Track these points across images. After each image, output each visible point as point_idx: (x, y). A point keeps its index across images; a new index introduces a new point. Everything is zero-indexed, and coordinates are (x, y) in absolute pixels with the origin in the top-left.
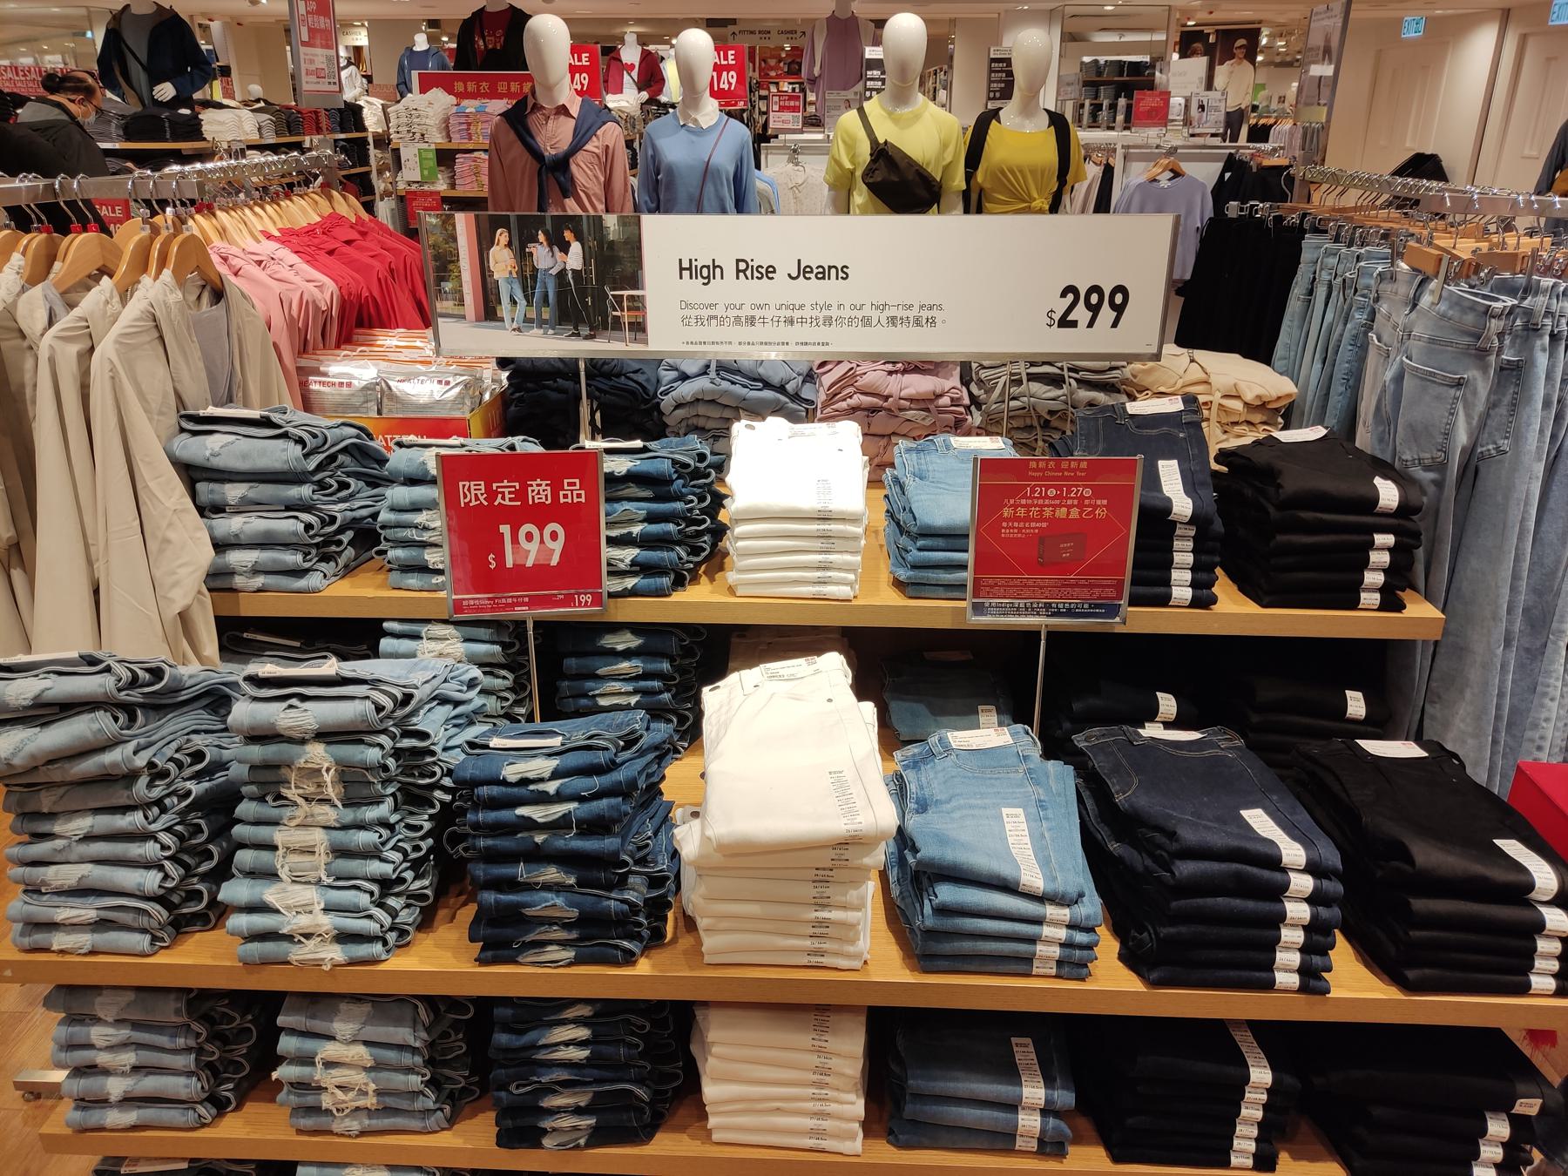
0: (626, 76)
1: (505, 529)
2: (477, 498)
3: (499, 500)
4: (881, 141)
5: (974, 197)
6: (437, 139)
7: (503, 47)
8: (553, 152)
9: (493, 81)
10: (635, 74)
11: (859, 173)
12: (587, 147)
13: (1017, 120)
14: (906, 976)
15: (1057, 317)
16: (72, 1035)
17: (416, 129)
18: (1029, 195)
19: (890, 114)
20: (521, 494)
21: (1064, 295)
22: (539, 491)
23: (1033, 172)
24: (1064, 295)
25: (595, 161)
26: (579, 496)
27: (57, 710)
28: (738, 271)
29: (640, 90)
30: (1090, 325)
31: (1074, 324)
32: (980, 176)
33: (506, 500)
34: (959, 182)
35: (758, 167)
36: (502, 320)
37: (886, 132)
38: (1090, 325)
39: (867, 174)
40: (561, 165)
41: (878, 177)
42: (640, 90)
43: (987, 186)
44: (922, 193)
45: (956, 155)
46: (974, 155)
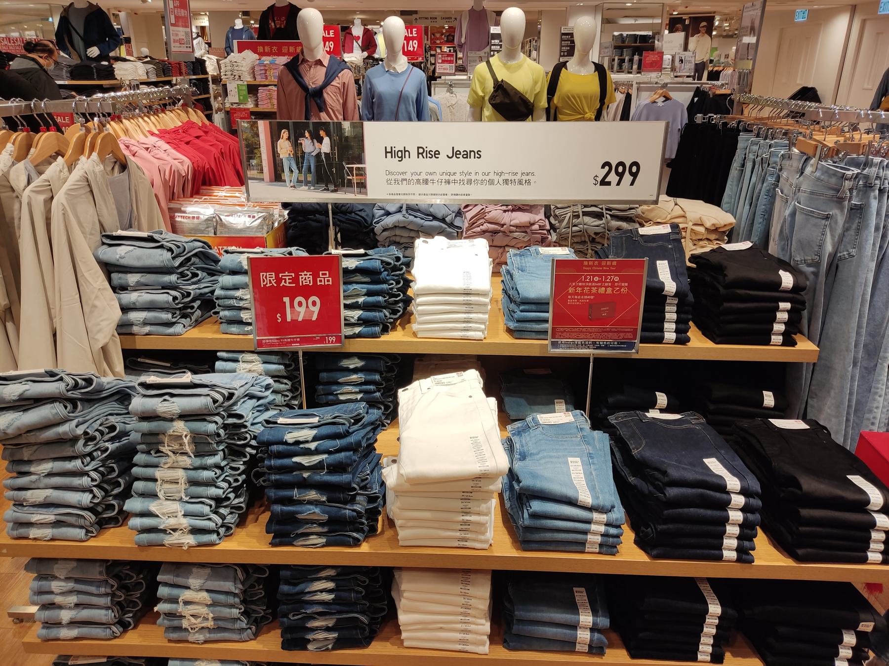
0: (355, 43)
1: (286, 300)
2: (270, 282)
3: (283, 283)
4: (500, 80)
5: (552, 112)
6: (248, 79)
7: (285, 27)
8: (314, 86)
9: (280, 46)
10: (360, 42)
11: (487, 98)
12: (333, 83)
13: (577, 68)
14: (514, 553)
15: (599, 179)
16: (41, 586)
17: (236, 73)
18: (584, 110)
19: (505, 65)
20: (295, 280)
21: (603, 167)
22: (306, 278)
23: (586, 97)
24: (603, 167)
25: (338, 91)
26: (328, 281)
27: (32, 402)
28: (419, 153)
29: (363, 51)
30: (618, 184)
31: (609, 184)
32: (556, 100)
33: (287, 283)
34: (544, 103)
35: (430, 94)
37: (502, 75)
38: (618, 184)
39: (492, 98)
40: (318, 93)
41: (498, 100)
42: (363, 51)
43: (560, 105)
44: (523, 109)
45: (542, 88)
46: (552, 88)
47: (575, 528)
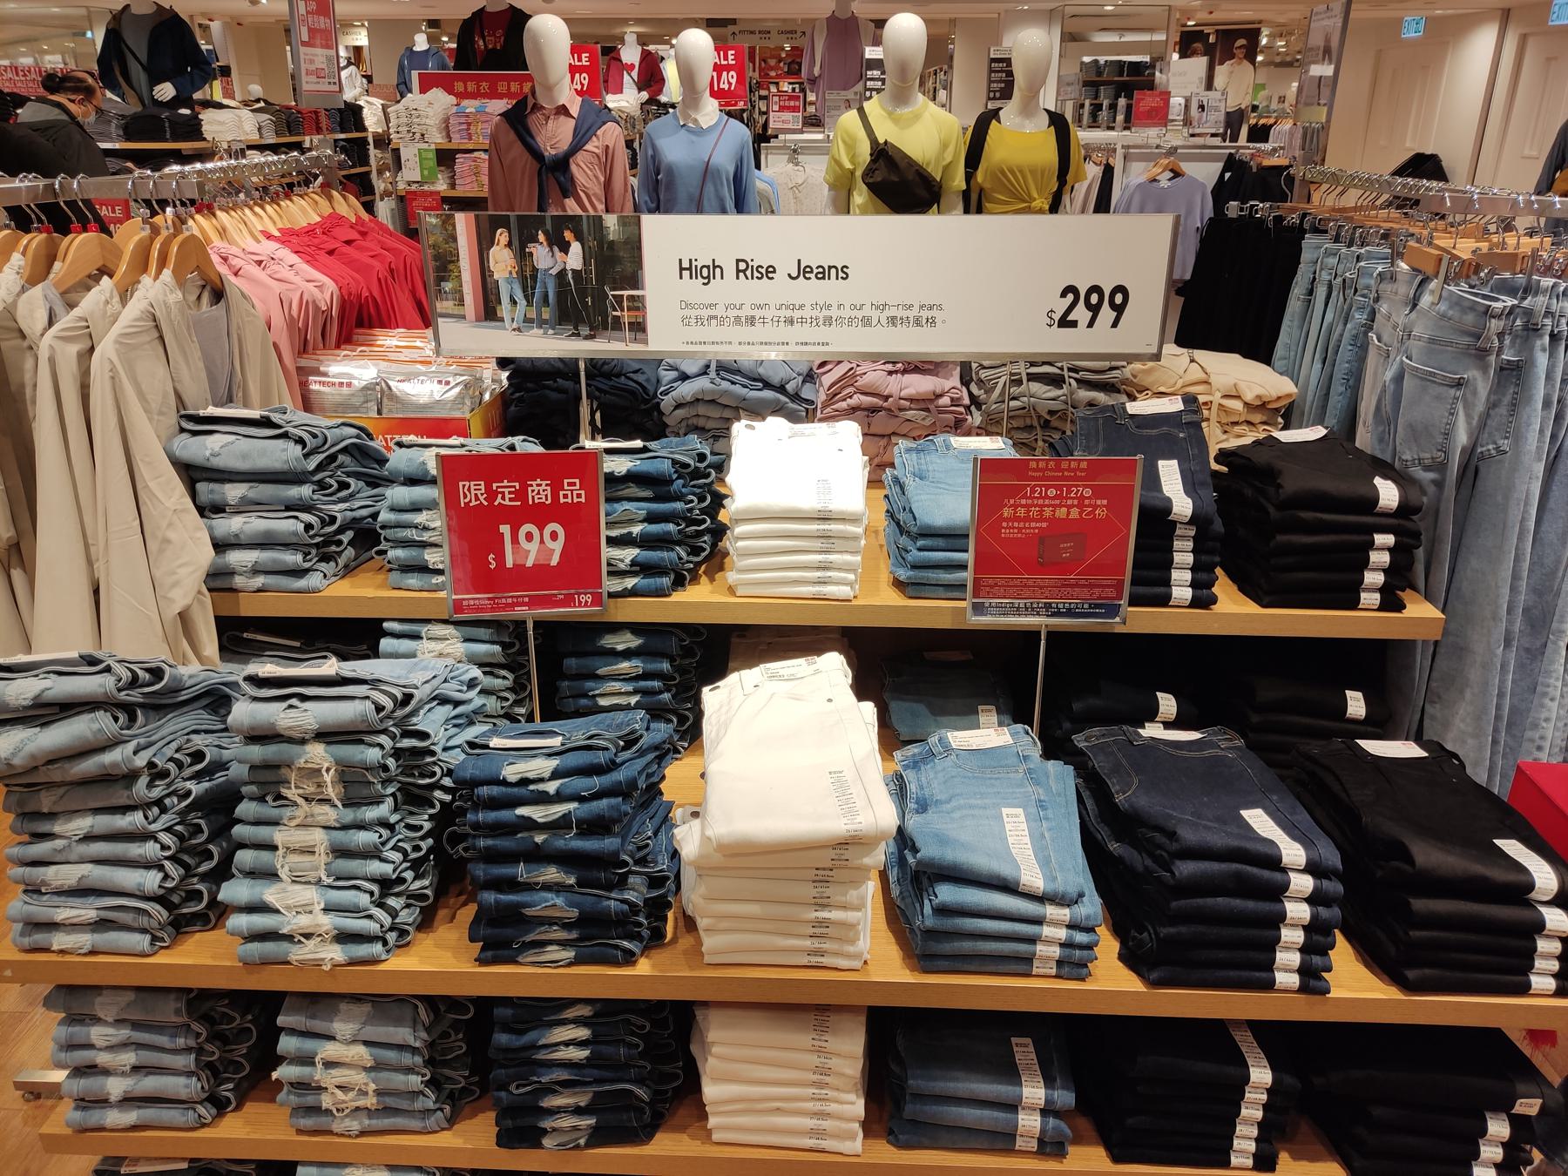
0: (626, 76)
1: (505, 529)
2: (477, 498)
3: (499, 500)
4: (881, 141)
5: (974, 197)
6: (437, 139)
7: (503, 47)
8: (553, 152)
9: (493, 81)
10: (635, 74)
11: (859, 173)
12: (587, 147)
13: (1017, 120)
14: (906, 976)
15: (1057, 317)
17: (416, 129)
18: (1029, 195)
19: (890, 114)
20: (521, 494)
21: (1064, 295)
22: (539, 491)
23: (1033, 172)
24: (1064, 295)
25: (595, 161)
26: (579, 496)
27: (57, 710)
28: (738, 271)
29: (640, 90)
30: (1090, 325)
31: (1074, 324)
32: (980, 176)
33: (506, 500)
34: (959, 182)
35: (758, 167)
36: (502, 320)
37: (886, 132)
38: (1090, 325)
39: (867, 174)
40: (561, 165)
41: (878, 177)
42: (640, 90)
43: (987, 186)
44: (922, 193)
45: (956, 155)
46: (974, 155)
47: (1015, 932)
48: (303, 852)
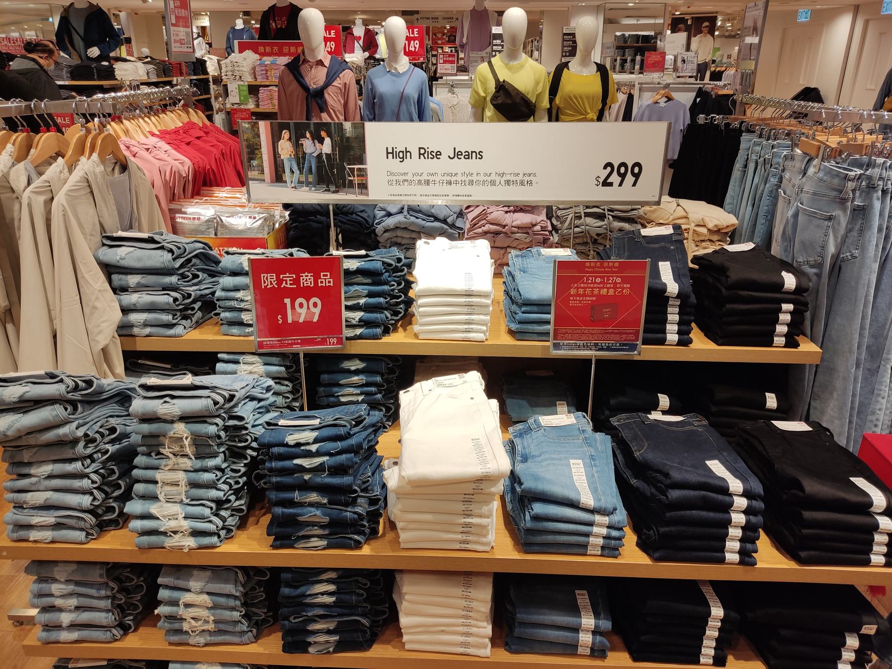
0: (356, 43)
1: (287, 301)
2: (271, 284)
3: (284, 284)
4: (501, 80)
5: (554, 112)
6: (249, 79)
7: (286, 27)
8: (315, 87)
9: (281, 46)
10: (361, 42)
11: (488, 99)
12: (334, 84)
13: (579, 68)
14: (515, 555)
15: (601, 180)
17: (237, 73)
18: (586, 111)
19: (506, 65)
20: (296, 281)
21: (605, 168)
22: (307, 279)
23: (588, 98)
24: (605, 168)
25: (339, 91)
26: (329, 282)
27: (32, 404)
28: (420, 154)
29: (364, 51)
30: (620, 185)
31: (611, 184)
32: (557, 100)
33: (288, 285)
34: (545, 103)
35: (431, 95)
36: (286, 182)
37: (504, 75)
38: (620, 185)
39: (493, 99)
40: (319, 94)
41: (500, 101)
42: (364, 51)
43: (561, 106)
44: (525, 110)
45: (544, 88)
46: (554, 88)
47: (577, 530)
48: (172, 485)
